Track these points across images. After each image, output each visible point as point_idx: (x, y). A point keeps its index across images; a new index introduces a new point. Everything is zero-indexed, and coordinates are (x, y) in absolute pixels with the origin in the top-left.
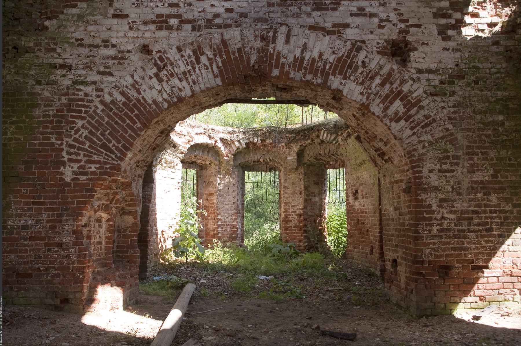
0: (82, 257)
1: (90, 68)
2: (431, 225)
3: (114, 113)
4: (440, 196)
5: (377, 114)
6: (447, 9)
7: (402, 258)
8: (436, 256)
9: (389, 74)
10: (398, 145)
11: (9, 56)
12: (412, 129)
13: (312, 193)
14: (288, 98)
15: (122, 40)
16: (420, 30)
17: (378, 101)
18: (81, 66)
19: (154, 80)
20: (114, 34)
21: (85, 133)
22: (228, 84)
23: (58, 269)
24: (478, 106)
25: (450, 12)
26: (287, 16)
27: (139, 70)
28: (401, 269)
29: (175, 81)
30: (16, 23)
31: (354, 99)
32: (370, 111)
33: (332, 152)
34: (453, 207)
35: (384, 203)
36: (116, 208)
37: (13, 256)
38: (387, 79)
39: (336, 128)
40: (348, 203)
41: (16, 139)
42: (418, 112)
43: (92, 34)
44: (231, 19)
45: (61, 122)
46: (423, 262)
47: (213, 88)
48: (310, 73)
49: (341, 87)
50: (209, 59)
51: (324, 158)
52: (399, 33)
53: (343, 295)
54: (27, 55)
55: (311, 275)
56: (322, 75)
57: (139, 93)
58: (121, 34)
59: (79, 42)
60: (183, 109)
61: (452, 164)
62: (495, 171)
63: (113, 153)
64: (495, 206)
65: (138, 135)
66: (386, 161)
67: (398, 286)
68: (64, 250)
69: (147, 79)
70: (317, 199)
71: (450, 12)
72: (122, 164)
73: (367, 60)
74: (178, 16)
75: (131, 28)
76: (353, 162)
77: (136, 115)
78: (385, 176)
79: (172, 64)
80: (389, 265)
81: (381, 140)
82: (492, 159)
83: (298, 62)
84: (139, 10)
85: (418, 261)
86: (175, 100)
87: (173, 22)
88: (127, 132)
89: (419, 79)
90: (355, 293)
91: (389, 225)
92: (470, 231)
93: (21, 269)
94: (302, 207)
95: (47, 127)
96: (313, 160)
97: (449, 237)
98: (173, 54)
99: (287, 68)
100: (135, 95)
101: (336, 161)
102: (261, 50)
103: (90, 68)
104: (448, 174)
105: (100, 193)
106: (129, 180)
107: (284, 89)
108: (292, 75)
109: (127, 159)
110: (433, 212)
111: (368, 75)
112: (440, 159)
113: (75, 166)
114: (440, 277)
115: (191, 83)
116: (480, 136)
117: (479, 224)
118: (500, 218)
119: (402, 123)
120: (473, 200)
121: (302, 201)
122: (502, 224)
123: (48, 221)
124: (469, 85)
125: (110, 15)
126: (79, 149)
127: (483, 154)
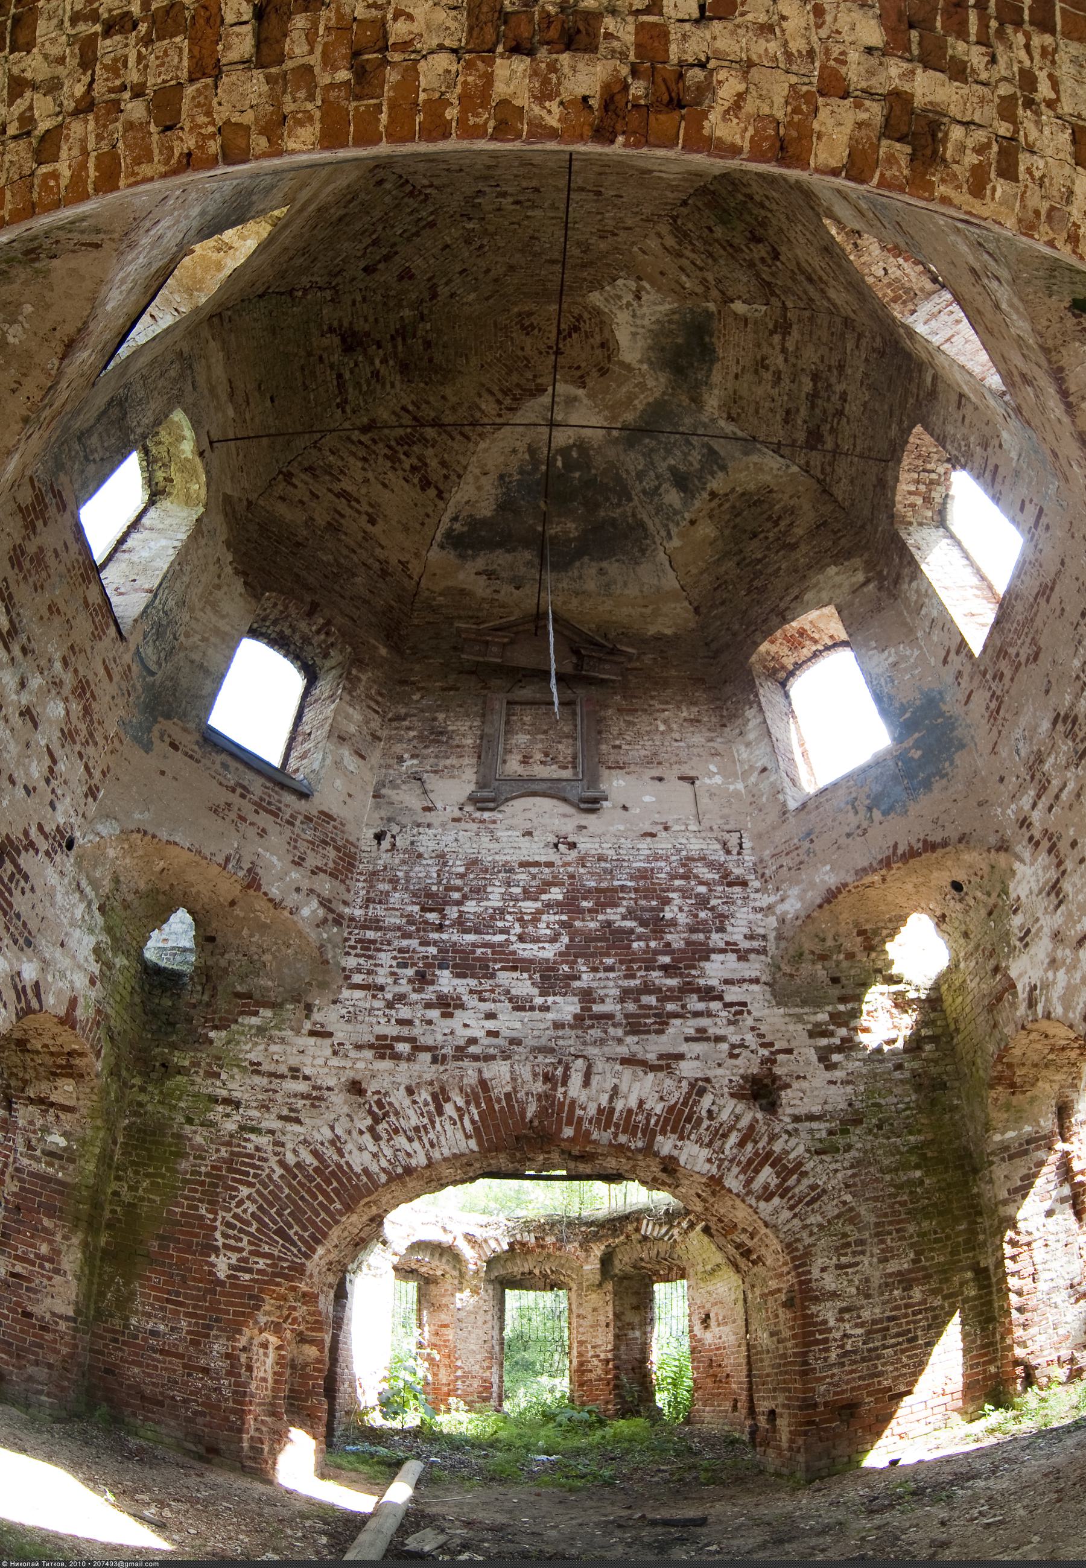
0: (241, 1394)
1: (268, 1108)
2: (827, 1350)
3: (299, 1182)
4: (839, 1304)
5: (735, 1191)
6: (827, 1024)
7: (784, 1406)
8: (836, 1393)
9: (751, 1127)
10: (771, 1236)
11: (154, 1076)
12: (791, 1208)
13: (629, 1324)
14: (588, 1171)
15: (321, 1071)
16: (792, 1057)
17: (735, 1170)
18: (254, 1104)
19: (367, 1138)
20: (308, 1061)
21: (252, 1208)
22: (489, 1148)
23: (203, 1404)
24: (886, 1162)
25: (831, 1027)
26: (585, 1043)
27: (344, 1120)
28: (782, 1423)
29: (401, 1141)
30: (170, 1029)
31: (697, 1169)
32: (723, 1187)
33: (662, 1255)
34: (859, 1317)
35: (752, 1328)
36: (293, 1330)
37: (136, 1370)
38: (749, 1136)
39: (670, 1217)
40: (693, 1337)
41: (150, 1200)
42: (799, 1181)
43: (275, 1057)
44: (495, 1047)
45: (216, 1186)
46: (816, 1405)
47: (463, 1155)
48: (624, 1132)
49: (675, 1153)
50: (458, 1109)
51: (649, 1266)
52: (762, 1063)
53: (686, 1475)
54: (179, 1078)
55: (627, 1451)
56: (644, 1136)
57: (342, 1156)
58: (320, 1061)
59: (256, 1068)
60: (410, 1185)
61: (855, 1254)
62: (917, 1253)
63: (295, 1245)
64: (919, 1304)
65: (337, 1222)
66: (754, 1263)
67: (779, 1448)
68: (212, 1379)
69: (355, 1134)
70: (638, 1334)
71: (831, 1027)
72: (308, 1263)
73: (715, 1108)
74: (411, 1040)
75: (335, 1053)
76: (700, 1268)
77: (334, 1190)
78: (753, 1286)
79: (397, 1113)
80: (762, 1421)
81: (744, 1230)
82: (911, 1237)
83: (605, 1116)
84: (349, 1027)
85: (808, 1405)
86: (400, 1170)
87: (403, 1048)
88: (318, 1215)
89: (796, 1130)
90: (706, 1470)
91: (762, 1360)
92: (885, 1347)
93: (148, 1391)
94: (610, 1347)
95: (196, 1191)
96: (629, 1269)
97: (855, 1362)
98: (399, 1098)
99: (586, 1125)
100: (335, 1157)
101: (670, 1269)
102: (545, 1098)
103: (268, 1108)
104: (850, 1270)
105: (269, 1304)
106: (315, 1290)
107: (583, 1157)
108: (595, 1136)
109: (316, 1257)
110: (829, 1330)
111: (717, 1131)
112: (837, 1249)
113: (234, 1257)
114: (842, 1421)
115: (427, 1146)
116: (891, 1206)
117: (898, 1335)
118: (927, 1319)
119: (776, 1200)
120: (888, 1302)
121: (611, 1337)
122: (930, 1327)
123: (188, 1332)
124: (870, 1131)
125: (304, 1031)
126: (241, 1231)
127: (898, 1231)
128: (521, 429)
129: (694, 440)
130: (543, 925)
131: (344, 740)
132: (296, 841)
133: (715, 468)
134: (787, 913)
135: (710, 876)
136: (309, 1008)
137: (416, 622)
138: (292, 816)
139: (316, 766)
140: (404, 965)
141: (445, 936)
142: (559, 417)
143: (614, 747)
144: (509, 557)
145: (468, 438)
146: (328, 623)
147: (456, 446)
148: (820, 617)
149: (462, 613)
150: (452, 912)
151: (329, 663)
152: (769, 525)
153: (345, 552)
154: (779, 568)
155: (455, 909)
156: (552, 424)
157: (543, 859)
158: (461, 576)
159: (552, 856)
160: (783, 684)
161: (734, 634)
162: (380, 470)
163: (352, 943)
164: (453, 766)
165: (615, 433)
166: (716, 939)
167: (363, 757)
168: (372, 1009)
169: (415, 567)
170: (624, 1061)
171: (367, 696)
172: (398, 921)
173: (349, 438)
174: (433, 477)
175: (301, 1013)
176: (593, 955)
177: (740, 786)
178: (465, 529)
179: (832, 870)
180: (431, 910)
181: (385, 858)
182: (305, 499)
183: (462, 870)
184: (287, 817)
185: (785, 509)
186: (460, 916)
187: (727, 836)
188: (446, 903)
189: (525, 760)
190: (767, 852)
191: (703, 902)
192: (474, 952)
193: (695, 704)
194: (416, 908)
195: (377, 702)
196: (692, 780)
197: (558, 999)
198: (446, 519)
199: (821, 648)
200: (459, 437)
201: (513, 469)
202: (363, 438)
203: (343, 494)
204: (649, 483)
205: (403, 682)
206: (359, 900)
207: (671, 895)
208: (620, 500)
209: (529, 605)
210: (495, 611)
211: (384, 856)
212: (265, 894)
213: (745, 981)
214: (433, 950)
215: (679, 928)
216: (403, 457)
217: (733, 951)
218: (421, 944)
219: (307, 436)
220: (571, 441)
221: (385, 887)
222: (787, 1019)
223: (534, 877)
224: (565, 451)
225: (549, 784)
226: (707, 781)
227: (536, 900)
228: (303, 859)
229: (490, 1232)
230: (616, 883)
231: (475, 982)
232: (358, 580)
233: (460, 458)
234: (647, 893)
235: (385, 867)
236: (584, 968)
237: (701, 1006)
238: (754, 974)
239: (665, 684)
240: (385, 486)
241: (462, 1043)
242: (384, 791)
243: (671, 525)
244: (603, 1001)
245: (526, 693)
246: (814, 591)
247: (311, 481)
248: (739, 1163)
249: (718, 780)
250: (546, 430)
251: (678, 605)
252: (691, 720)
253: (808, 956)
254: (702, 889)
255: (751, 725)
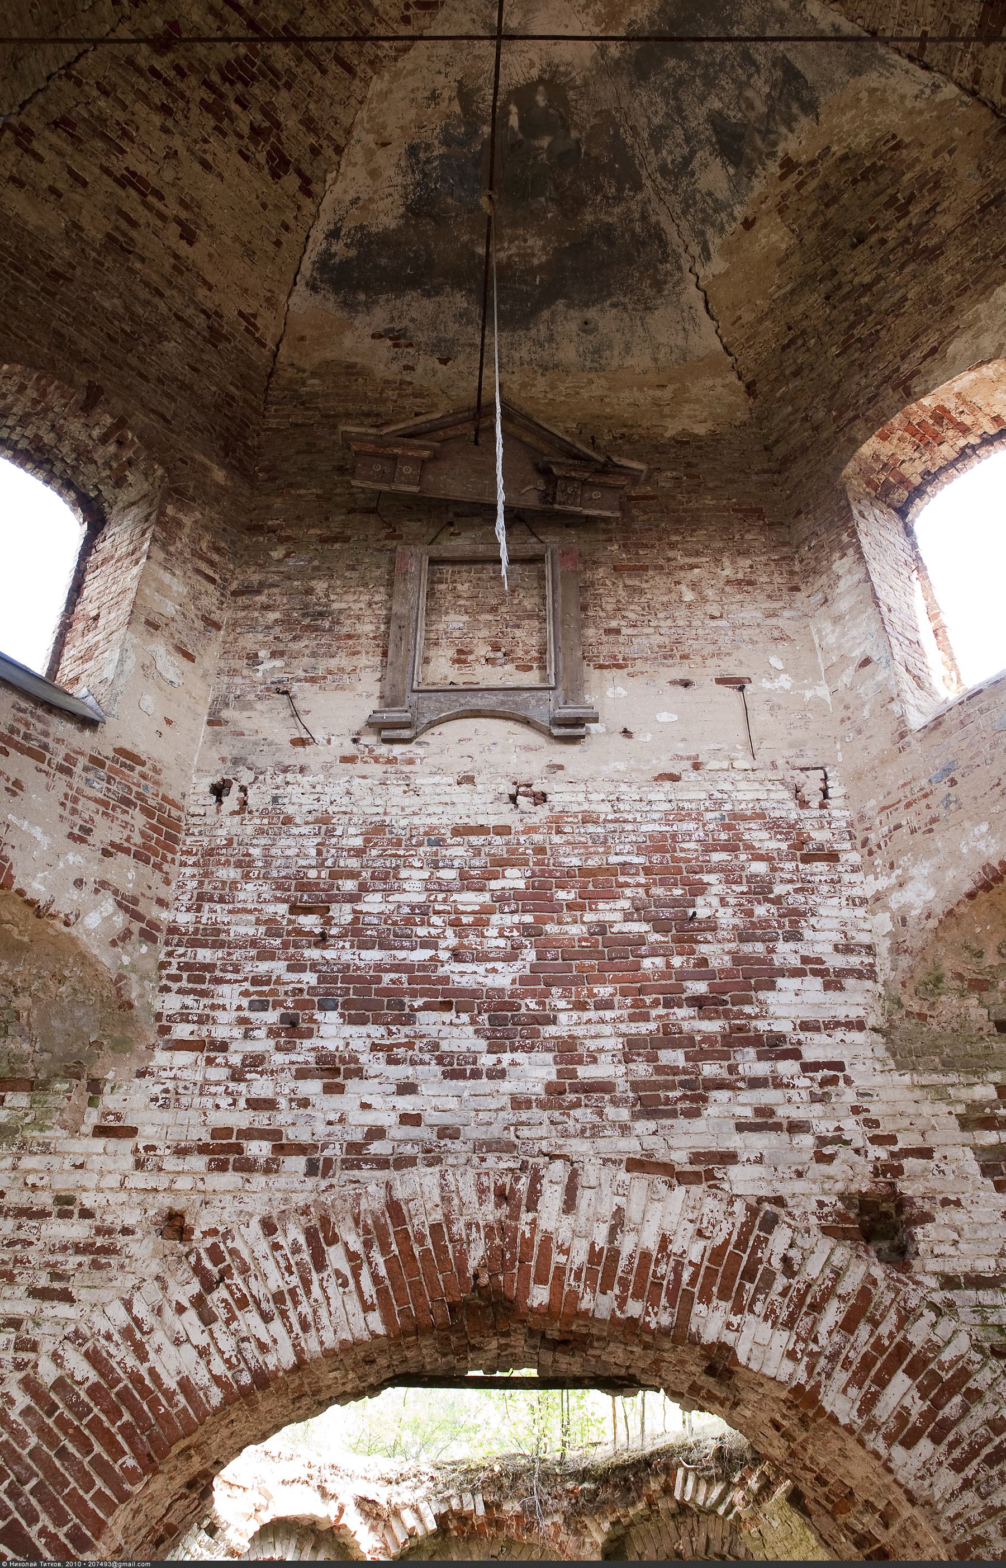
3: (61, 1422)
5: (844, 1420)
6: (990, 1103)
9: (864, 1294)
12: (958, 1466)
14: (576, 1370)
26: (565, 1134)
27: (151, 1287)
31: (770, 1371)
32: (821, 1410)
42: (965, 1410)
43: (31, 1179)
44: (415, 1142)
47: (358, 1343)
48: (637, 1296)
49: (729, 1338)
50: (352, 1256)
52: (876, 1173)
57: (143, 1357)
65: (124, 1497)
69: (169, 1312)
73: (794, 1254)
74: (273, 1135)
75: (139, 1165)
77: (123, 1429)
79: (244, 1270)
84: (166, 1117)
86: (246, 1379)
87: (259, 1149)
89: (950, 1305)
100: (131, 1361)
107: (566, 1344)
108: (585, 1304)
111: (802, 1298)
115: (297, 1328)
119: (925, 1447)
125: (87, 1129)
128: (444, 48)
129: (760, 52)
130: (493, 932)
131: (156, 627)
132: (75, 800)
133: (795, 109)
134: (911, 906)
135: (773, 845)
136: (95, 1087)
137: (273, 423)
138: (67, 758)
139: (109, 672)
140: (263, 1006)
141: (330, 954)
142: (513, 22)
143: (609, 631)
144: (429, 305)
145: (349, 69)
146: (121, 423)
147: (329, 86)
148: (975, 383)
149: (351, 407)
150: (342, 914)
151: (125, 496)
152: (890, 215)
153: (144, 294)
154: (904, 299)
155: (347, 907)
156: (501, 36)
157: (491, 821)
158: (348, 340)
159: (507, 816)
160: (902, 512)
161: (816, 428)
162: (195, 133)
163: (173, 970)
164: (342, 670)
165: (614, 50)
166: (786, 953)
167: (190, 657)
168: (207, 1082)
169: (268, 325)
170: (635, 1165)
171: (194, 553)
172: (251, 931)
173: (131, 62)
174: (294, 151)
175: (80, 1097)
176: (576, 982)
177: (823, 691)
178: (353, 253)
179: (991, 831)
180: (308, 911)
181: (231, 825)
182: (61, 186)
183: (358, 842)
184: (59, 759)
185: (921, 181)
186: (356, 920)
187: (800, 777)
188: (332, 899)
189: (461, 657)
190: (873, 802)
191: (761, 889)
192: (378, 980)
193: (744, 553)
194: (283, 908)
195: (212, 564)
196: (739, 684)
197: (520, 1056)
198: (318, 234)
199: (974, 440)
200: (334, 68)
201: (432, 135)
202: (160, 64)
203: (129, 180)
204: (670, 154)
205: (254, 529)
206: (185, 898)
207: (706, 878)
208: (620, 189)
209: (465, 391)
210: (407, 402)
211: (228, 821)
212: (21, 892)
213: (838, 1024)
214: (310, 978)
215: (721, 934)
216: (235, 108)
217: (815, 973)
218: (290, 969)
219: (50, 49)
220: (535, 73)
221: (232, 873)
222: (918, 1094)
223: (477, 852)
224: (523, 94)
225: (501, 696)
226: (767, 685)
227: (481, 890)
228: (88, 831)
229: (404, 1495)
230: (614, 859)
231: (382, 1030)
232: (169, 346)
233: (338, 110)
234: (666, 875)
235: (230, 842)
236: (562, 1004)
237: (762, 1069)
238: (854, 1013)
239: (694, 521)
240: (206, 165)
241: (358, 1136)
242: (226, 714)
243: (710, 232)
244: (595, 1061)
245: (461, 544)
246: (968, 336)
247: (69, 149)
248: (847, 1364)
249: (785, 681)
250: (487, 48)
251: (719, 381)
252: (739, 582)
253: (950, 983)
254: (760, 868)
255: (843, 585)
